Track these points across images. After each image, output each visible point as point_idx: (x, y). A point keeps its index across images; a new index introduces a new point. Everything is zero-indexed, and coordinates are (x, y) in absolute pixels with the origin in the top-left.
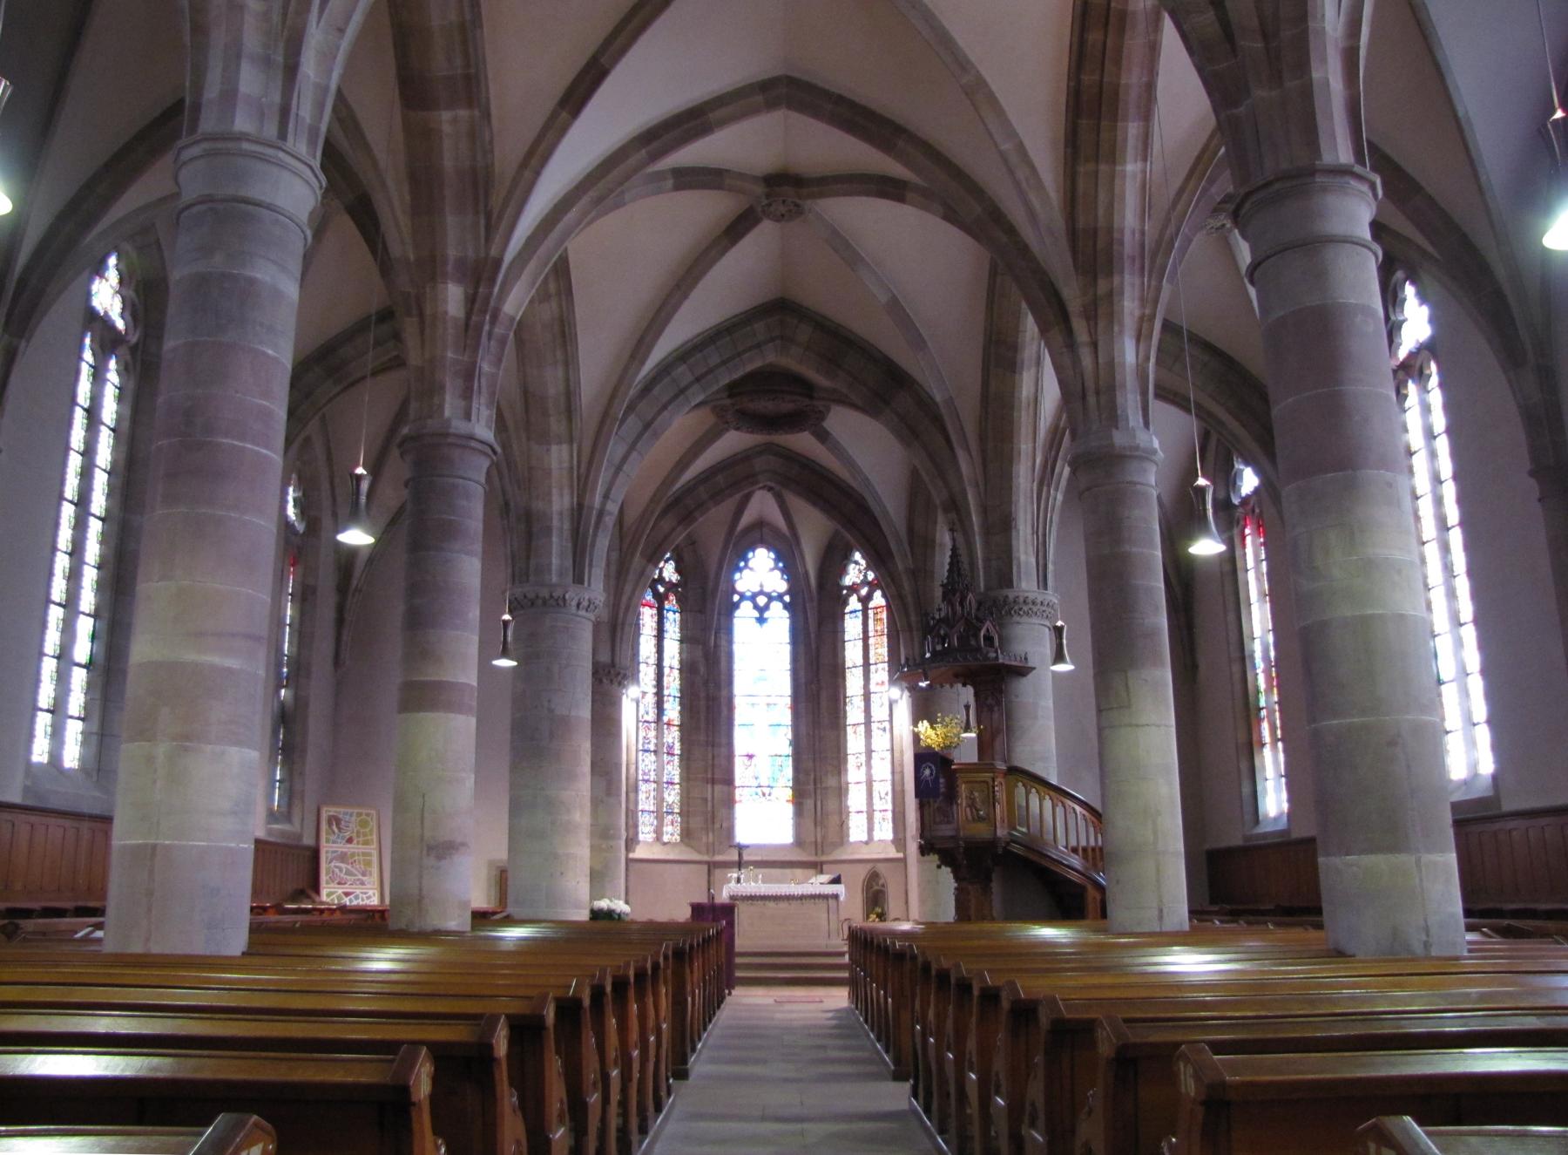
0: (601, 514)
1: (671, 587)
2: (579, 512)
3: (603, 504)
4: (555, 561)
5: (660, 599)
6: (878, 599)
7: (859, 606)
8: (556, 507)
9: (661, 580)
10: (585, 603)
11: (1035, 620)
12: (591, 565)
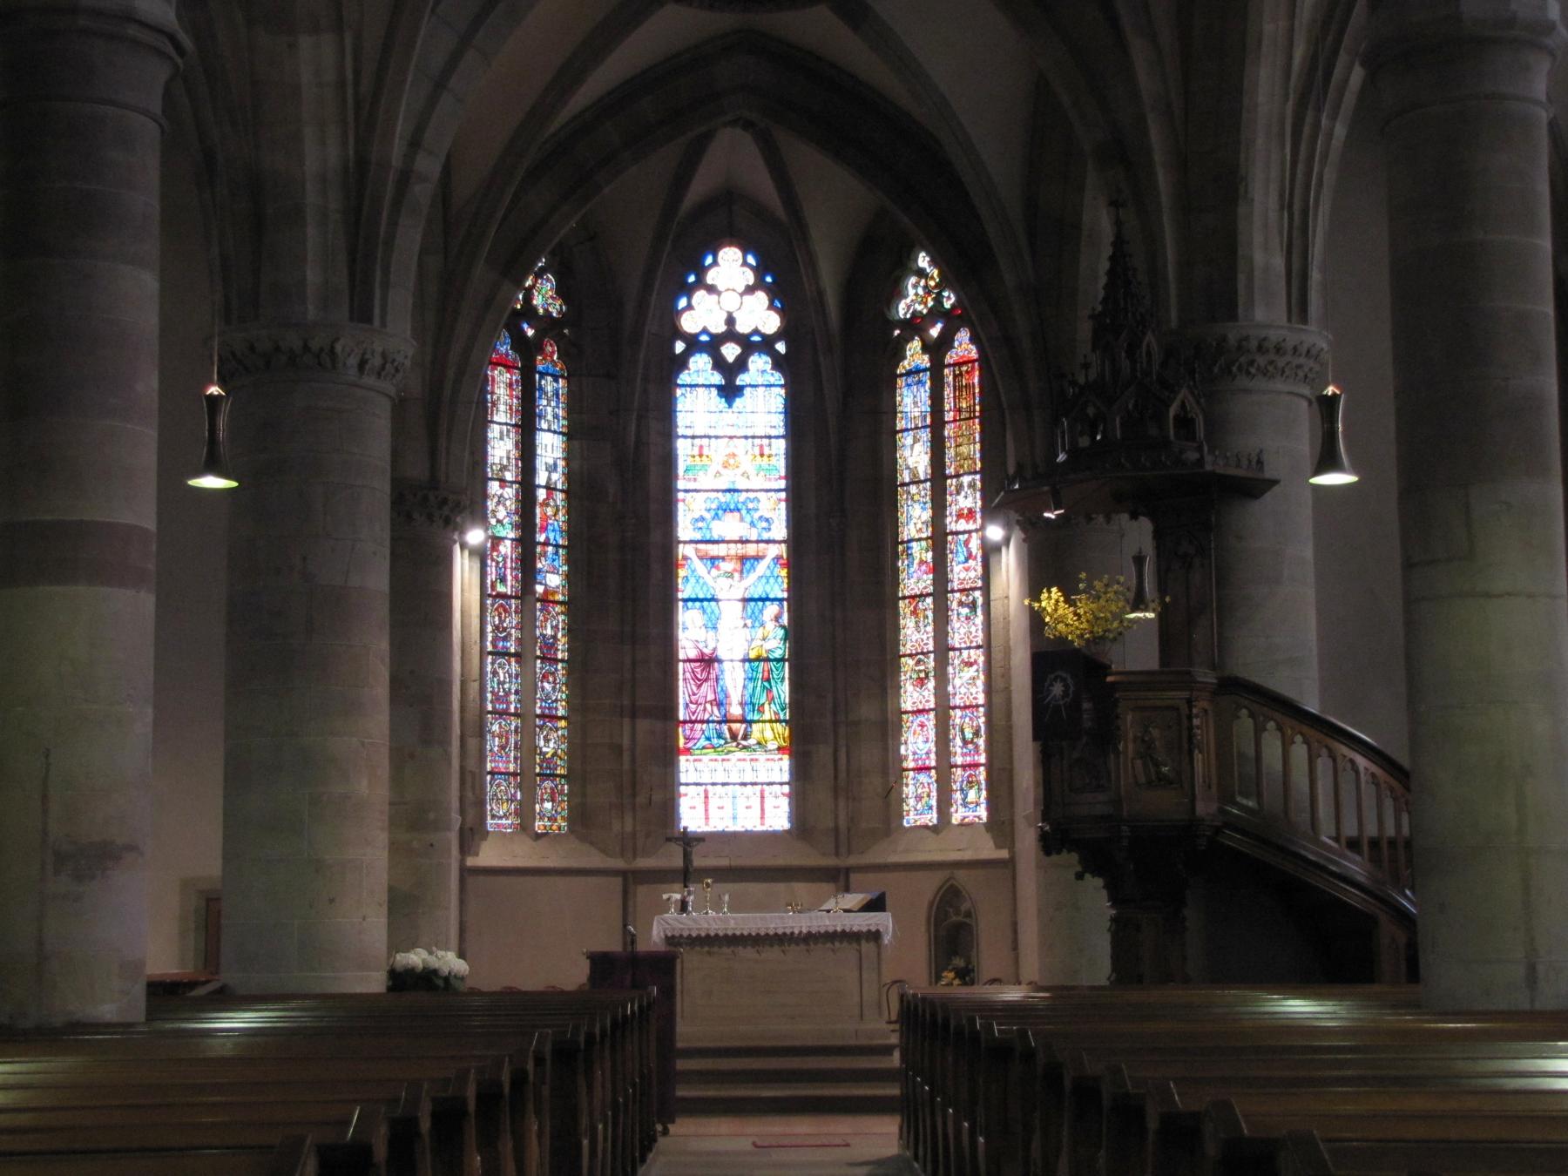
0: (405, 177)
1: (547, 325)
2: (358, 177)
3: (410, 156)
4: (312, 276)
5: (527, 350)
6: (964, 346)
7: (924, 361)
8: (311, 165)
9: (529, 312)
10: (377, 361)
11: (1279, 385)
12: (386, 285)
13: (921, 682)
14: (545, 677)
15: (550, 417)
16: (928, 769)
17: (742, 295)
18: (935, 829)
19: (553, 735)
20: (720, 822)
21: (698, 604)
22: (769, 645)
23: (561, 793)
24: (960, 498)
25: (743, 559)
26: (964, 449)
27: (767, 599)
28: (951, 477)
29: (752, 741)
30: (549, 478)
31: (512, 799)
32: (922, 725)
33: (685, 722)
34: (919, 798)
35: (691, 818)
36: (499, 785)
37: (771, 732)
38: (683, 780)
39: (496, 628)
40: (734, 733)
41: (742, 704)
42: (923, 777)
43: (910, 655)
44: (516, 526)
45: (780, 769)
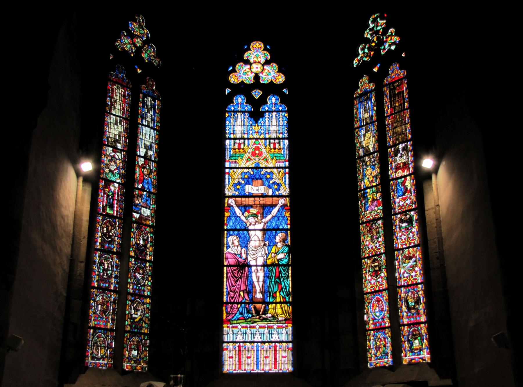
13: (376, 273)
14: (137, 270)
15: (149, 119)
16: (384, 328)
17: (263, 65)
18: (391, 368)
19: (141, 307)
20: (248, 366)
21: (236, 232)
22: (280, 256)
23: (145, 345)
24: (398, 158)
25: (263, 206)
26: (399, 129)
27: (278, 229)
28: (391, 147)
29: (269, 315)
30: (146, 153)
31: (109, 347)
32: (378, 301)
33: (227, 303)
34: (378, 348)
35: (230, 365)
36: (99, 337)
37: (279, 310)
38: (225, 340)
39: (104, 235)
40: (256, 311)
41: (262, 292)
42: (380, 335)
43: (369, 258)
44: (122, 176)
45: (285, 333)
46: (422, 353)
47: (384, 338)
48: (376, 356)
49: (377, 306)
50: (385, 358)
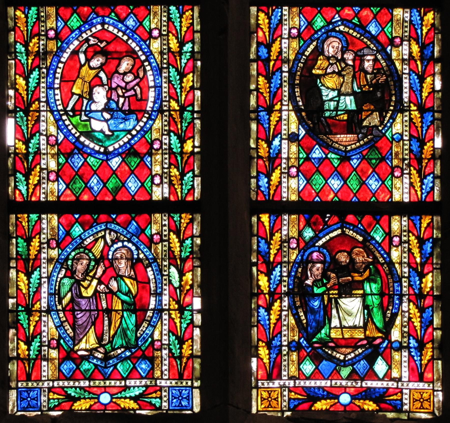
46: (380, 367)
47: (135, 263)
48: (69, 355)
49: (96, 82)
50: (133, 374)
